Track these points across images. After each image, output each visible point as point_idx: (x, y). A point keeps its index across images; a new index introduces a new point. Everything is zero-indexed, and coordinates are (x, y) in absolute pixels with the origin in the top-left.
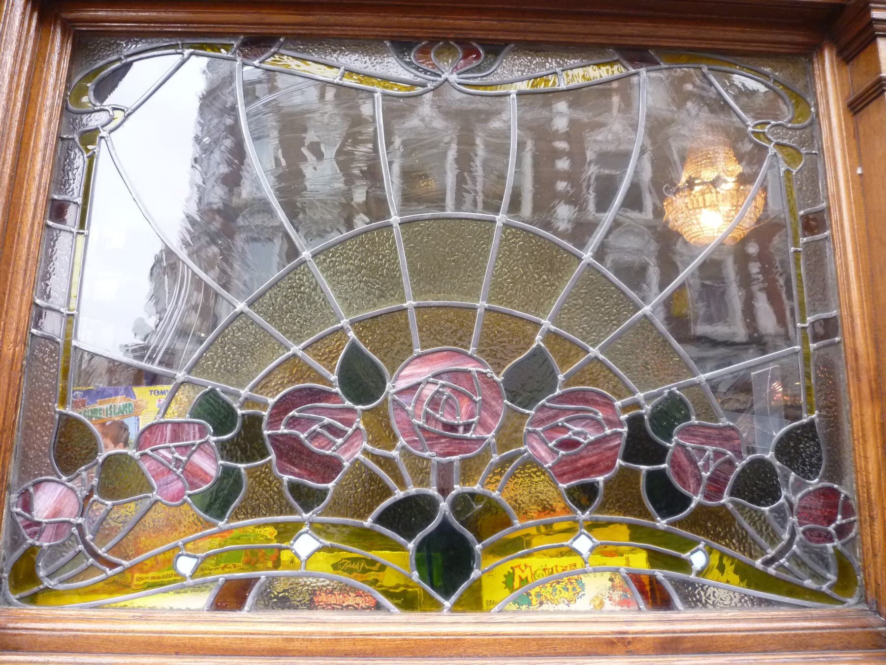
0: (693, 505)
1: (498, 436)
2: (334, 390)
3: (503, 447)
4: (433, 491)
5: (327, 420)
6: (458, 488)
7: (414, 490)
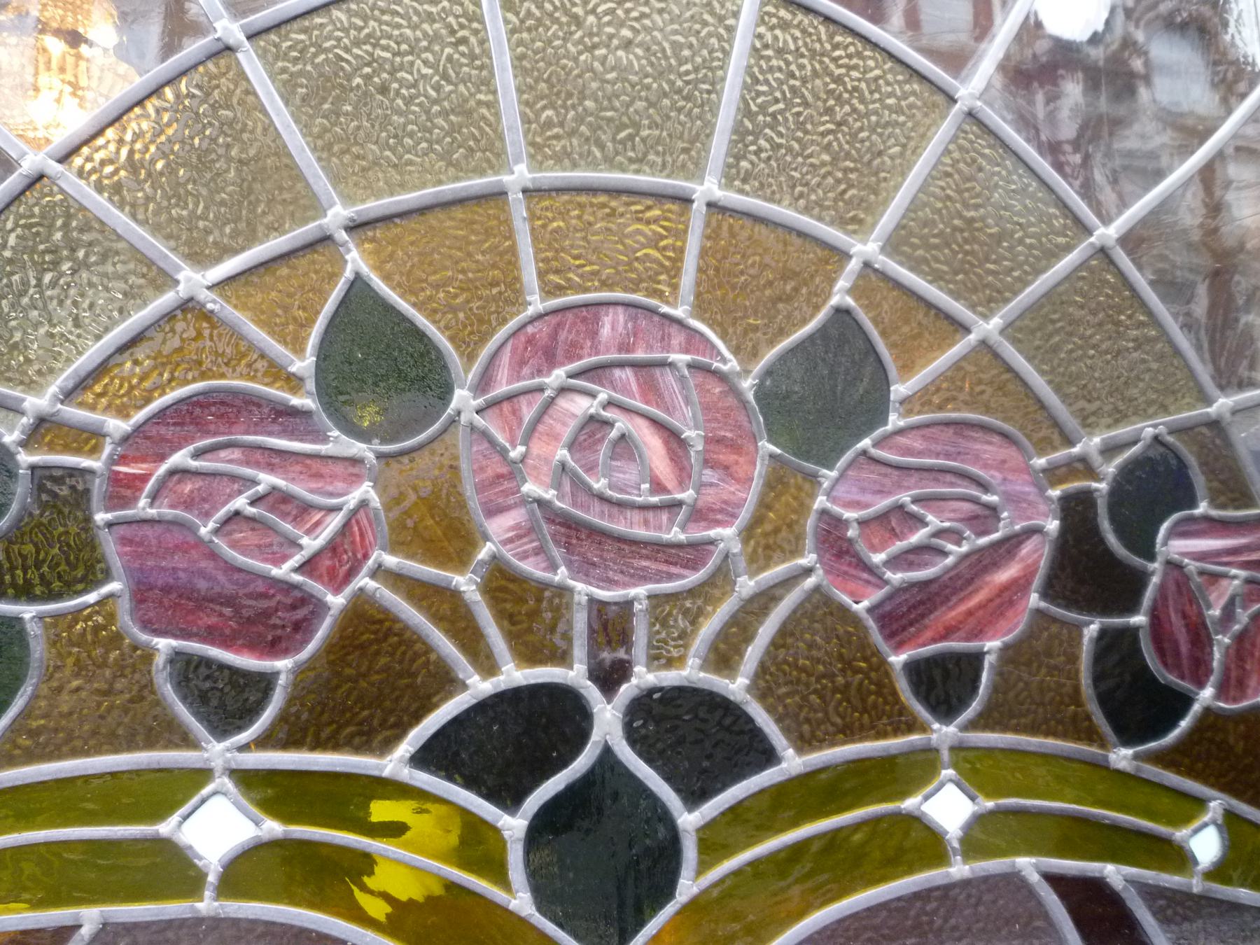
0: (1196, 708)
1: (747, 534)
2: (296, 401)
3: (758, 560)
4: (576, 674)
5: (267, 480)
6: (643, 677)
7: (752, 583)
